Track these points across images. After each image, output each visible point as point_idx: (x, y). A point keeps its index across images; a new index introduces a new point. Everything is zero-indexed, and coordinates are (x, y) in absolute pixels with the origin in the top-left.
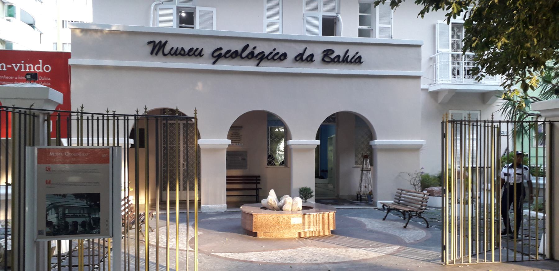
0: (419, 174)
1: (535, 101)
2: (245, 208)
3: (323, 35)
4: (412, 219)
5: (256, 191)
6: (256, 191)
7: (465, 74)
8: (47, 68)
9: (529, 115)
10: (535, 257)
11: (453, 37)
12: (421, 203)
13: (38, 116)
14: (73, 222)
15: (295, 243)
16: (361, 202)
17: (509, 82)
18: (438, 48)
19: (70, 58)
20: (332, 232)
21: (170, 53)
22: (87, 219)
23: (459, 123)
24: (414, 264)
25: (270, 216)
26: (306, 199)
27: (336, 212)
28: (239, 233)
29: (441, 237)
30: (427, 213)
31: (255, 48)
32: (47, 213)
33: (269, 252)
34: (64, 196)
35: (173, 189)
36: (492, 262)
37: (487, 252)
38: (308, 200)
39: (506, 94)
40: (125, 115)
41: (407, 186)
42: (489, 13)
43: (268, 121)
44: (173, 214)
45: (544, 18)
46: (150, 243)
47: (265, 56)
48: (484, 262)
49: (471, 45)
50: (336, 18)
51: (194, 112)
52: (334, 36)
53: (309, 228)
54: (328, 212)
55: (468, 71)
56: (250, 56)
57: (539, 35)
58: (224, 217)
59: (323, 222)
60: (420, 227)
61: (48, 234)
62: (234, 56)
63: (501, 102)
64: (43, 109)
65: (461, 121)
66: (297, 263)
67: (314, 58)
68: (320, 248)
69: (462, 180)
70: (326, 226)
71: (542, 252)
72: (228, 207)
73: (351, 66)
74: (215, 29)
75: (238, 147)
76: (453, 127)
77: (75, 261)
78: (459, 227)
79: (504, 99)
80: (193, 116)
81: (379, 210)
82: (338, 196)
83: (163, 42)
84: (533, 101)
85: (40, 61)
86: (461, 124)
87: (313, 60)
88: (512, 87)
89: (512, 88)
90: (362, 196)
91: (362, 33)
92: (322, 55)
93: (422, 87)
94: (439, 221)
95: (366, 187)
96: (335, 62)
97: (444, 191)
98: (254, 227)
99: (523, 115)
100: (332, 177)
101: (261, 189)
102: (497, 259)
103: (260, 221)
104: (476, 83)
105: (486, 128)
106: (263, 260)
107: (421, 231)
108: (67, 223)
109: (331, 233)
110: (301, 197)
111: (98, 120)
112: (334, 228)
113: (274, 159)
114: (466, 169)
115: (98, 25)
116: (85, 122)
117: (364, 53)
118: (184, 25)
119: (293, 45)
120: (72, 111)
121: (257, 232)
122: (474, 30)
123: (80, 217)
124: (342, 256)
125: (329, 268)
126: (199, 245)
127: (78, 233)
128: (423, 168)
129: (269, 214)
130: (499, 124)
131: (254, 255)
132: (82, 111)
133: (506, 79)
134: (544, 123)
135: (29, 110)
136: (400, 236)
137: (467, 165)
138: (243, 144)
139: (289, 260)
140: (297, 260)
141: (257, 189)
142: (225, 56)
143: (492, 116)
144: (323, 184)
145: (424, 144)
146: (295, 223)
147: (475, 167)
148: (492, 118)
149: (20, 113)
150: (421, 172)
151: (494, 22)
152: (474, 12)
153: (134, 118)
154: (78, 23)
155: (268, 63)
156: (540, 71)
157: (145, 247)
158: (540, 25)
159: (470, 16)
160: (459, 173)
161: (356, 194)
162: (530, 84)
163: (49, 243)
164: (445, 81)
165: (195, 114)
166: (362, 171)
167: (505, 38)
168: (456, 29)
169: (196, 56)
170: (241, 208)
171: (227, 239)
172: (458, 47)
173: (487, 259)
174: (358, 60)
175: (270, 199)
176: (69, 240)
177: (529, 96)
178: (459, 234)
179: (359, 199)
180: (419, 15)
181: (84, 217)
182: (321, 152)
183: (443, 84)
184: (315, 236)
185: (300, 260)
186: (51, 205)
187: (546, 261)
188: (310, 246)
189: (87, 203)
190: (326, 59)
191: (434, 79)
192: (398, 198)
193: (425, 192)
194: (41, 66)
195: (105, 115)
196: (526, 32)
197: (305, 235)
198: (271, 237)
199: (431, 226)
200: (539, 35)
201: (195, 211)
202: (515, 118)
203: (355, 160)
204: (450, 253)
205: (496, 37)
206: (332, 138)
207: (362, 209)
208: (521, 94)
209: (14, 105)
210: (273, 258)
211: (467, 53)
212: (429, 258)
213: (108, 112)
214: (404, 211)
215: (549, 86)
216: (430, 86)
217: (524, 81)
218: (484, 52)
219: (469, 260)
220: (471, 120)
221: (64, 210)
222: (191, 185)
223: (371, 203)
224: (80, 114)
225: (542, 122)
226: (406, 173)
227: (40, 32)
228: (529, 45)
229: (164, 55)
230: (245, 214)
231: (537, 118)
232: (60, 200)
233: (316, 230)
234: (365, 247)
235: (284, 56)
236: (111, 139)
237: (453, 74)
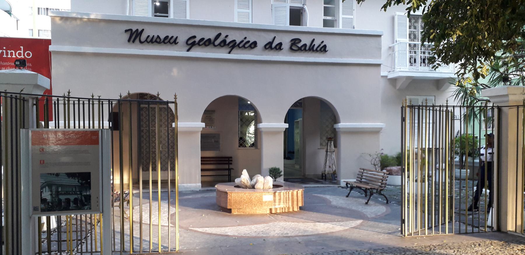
0: (379, 155)
1: (484, 88)
2: (220, 187)
3: (290, 25)
4: (372, 196)
5: (228, 171)
6: (228, 171)
7: (421, 63)
8: (28, 55)
9: (479, 100)
10: (484, 230)
11: (410, 27)
12: (381, 181)
13: (28, 101)
15: (267, 218)
16: (326, 181)
17: (462, 71)
18: (397, 38)
19: (51, 45)
20: (301, 208)
21: (146, 40)
23: (417, 108)
24: (376, 236)
26: (275, 178)
27: (304, 189)
28: (214, 209)
29: (400, 213)
30: (387, 190)
31: (227, 36)
32: (42, 191)
33: (243, 227)
34: (57, 175)
35: (155, 169)
36: (446, 233)
37: (441, 225)
38: (277, 179)
39: (459, 81)
40: (109, 100)
41: (368, 165)
42: (445, 8)
43: (239, 105)
44: (155, 193)
45: (494, 13)
46: (133, 220)
47: (237, 44)
48: (439, 233)
49: (429, 38)
50: (302, 9)
51: (68, 94)
52: (300, 25)
53: (279, 204)
54: (297, 190)
55: (424, 60)
56: (222, 44)
57: (489, 28)
58: (199, 196)
59: (293, 199)
60: (382, 204)
62: (207, 43)
63: (454, 88)
64: (33, 94)
65: (419, 106)
66: (270, 236)
67: (283, 47)
68: (290, 223)
69: (420, 161)
70: (295, 203)
71: (490, 225)
72: (202, 186)
73: (317, 54)
74: (188, 18)
75: (211, 130)
76: (411, 112)
77: (64, 237)
78: (416, 203)
79: (458, 86)
80: (174, 100)
81: (343, 188)
82: (304, 175)
83: (140, 30)
84: (483, 88)
85: (21, 47)
86: (419, 109)
87: (282, 48)
88: (465, 75)
89: (465, 76)
91: (326, 23)
92: (290, 44)
93: (382, 75)
94: (397, 198)
95: (330, 167)
96: (302, 50)
97: (403, 170)
98: (228, 204)
99: (473, 101)
100: (298, 158)
101: (233, 169)
102: (450, 231)
104: (431, 70)
105: (441, 112)
106: (238, 234)
107: (381, 207)
108: (60, 200)
109: (300, 209)
110: (271, 176)
111: (84, 104)
112: (302, 205)
113: (245, 141)
114: (423, 150)
115: (78, 13)
116: (71, 106)
117: (329, 42)
118: (158, 14)
119: (263, 34)
120: (53, 95)
122: (432, 23)
123: (72, 194)
124: (311, 230)
125: (300, 240)
126: (180, 220)
128: (383, 149)
129: (243, 192)
130: (452, 109)
131: (230, 230)
132: (69, 95)
133: (460, 68)
134: (493, 108)
135: (19, 95)
136: (363, 211)
137: (424, 147)
138: (215, 128)
139: (263, 234)
140: (270, 234)
141: (229, 170)
142: (199, 44)
143: (447, 101)
144: (290, 164)
145: (383, 127)
146: (266, 200)
147: (431, 149)
148: (447, 103)
149: (11, 98)
150: (381, 152)
151: (449, 16)
152: (432, 7)
153: (108, 102)
154: (58, 11)
155: (239, 51)
156: (490, 61)
157: (130, 221)
158: (490, 19)
159: (428, 11)
160: (417, 154)
162: (481, 73)
163: (40, 219)
164: (402, 68)
165: (175, 98)
166: (327, 152)
167: (459, 31)
168: (413, 21)
169: (171, 43)
170: (216, 186)
171: (204, 215)
172: (415, 37)
173: (441, 231)
174: (323, 49)
175: (243, 178)
176: (47, 217)
177: (479, 83)
178: (416, 209)
179: (324, 178)
180: (382, 8)
181: (76, 194)
182: (288, 135)
183: (401, 71)
184: (285, 212)
185: (272, 234)
186: (45, 184)
187: (494, 233)
188: (280, 221)
189: (78, 181)
190: (294, 48)
191: (393, 67)
192: (360, 178)
193: (385, 171)
194: (22, 52)
195: (90, 100)
196: (478, 26)
198: (245, 213)
199: (390, 202)
200: (489, 28)
201: (176, 190)
202: (467, 103)
203: (320, 142)
204: (408, 226)
205: (451, 30)
206: (298, 122)
207: (327, 187)
208: (473, 82)
209: (6, 90)
210: (247, 232)
211: (426, 43)
212: (389, 231)
213: (93, 96)
214: (366, 189)
215: (498, 74)
216: (389, 73)
217: (475, 70)
218: (440, 43)
219: (425, 232)
220: (428, 105)
221: (57, 188)
222: (154, 166)
223: (335, 181)
224: (67, 99)
225: (491, 107)
226: (367, 154)
227: (16, 18)
228: (480, 37)
229: (141, 42)
230: (219, 192)
231: (486, 104)
232: (54, 179)
233: (286, 206)
234: (331, 221)
235: (255, 44)
236: (72, 122)
237: (410, 62)
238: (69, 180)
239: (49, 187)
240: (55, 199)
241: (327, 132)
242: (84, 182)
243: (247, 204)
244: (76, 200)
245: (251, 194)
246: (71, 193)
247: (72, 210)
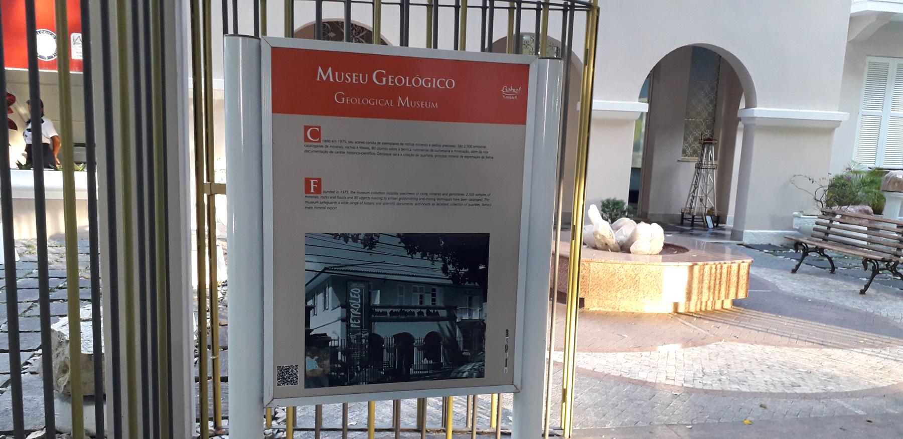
14: (398, 338)
20: (735, 303)
22: (445, 325)
25: (620, 265)
32: (310, 303)
34: (370, 241)
61: (313, 382)
90: (695, 217)
103: (596, 276)
108: (376, 341)
121: (584, 299)
127: (414, 375)
161: (681, 213)
181: (435, 318)
186: (323, 276)
189: (445, 270)
197: (686, 308)
238: (409, 261)
239: (336, 290)
240: (359, 339)
241: (697, 127)
242: (464, 271)
243: (625, 291)
244: (432, 338)
245: (636, 266)
246: (416, 311)
247: (418, 378)
